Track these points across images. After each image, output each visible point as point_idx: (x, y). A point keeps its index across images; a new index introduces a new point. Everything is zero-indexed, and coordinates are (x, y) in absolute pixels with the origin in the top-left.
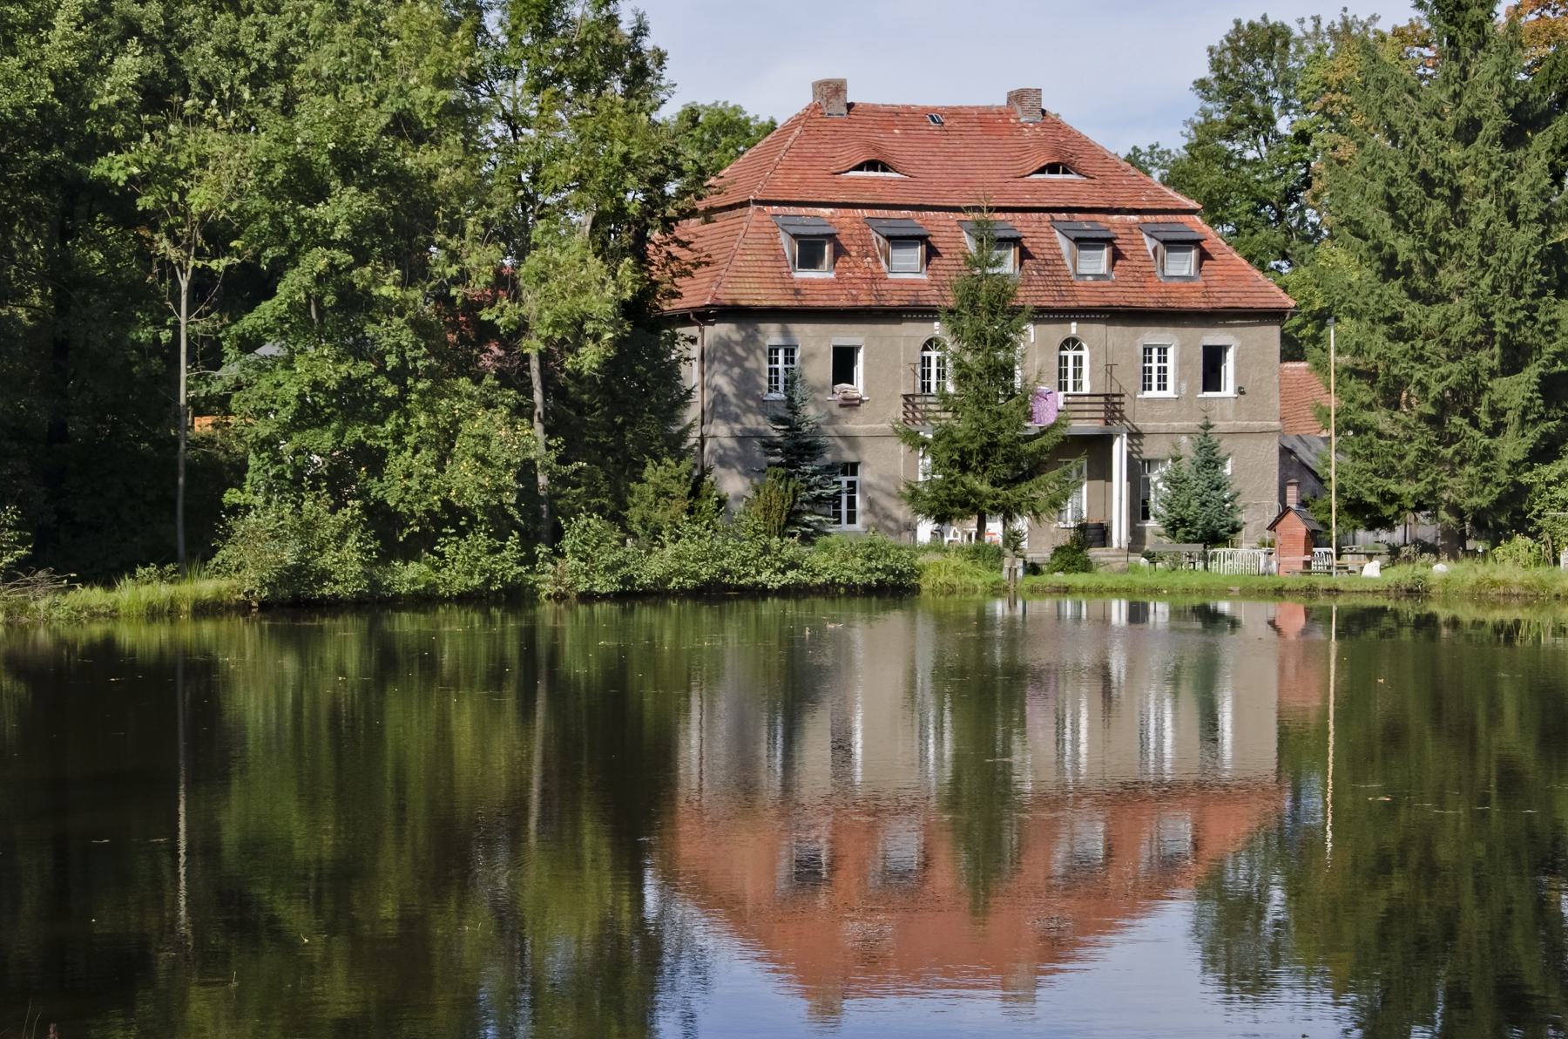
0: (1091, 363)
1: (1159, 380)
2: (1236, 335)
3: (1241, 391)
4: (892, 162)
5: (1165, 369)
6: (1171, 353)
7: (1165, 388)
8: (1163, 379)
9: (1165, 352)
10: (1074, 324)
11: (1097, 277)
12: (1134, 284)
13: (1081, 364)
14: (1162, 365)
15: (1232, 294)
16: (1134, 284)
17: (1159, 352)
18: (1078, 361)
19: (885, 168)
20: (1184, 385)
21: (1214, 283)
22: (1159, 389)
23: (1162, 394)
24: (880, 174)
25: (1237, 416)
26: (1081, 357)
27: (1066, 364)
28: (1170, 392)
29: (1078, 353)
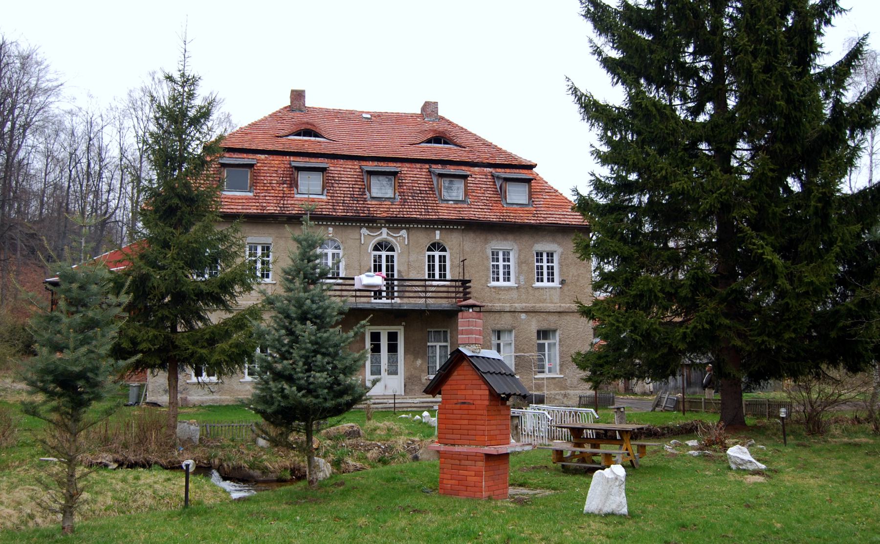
0: (451, 260)
1: (548, 275)
2: (559, 244)
3: (563, 282)
4: (323, 133)
5: (552, 268)
6: (556, 258)
7: (553, 281)
8: (508, 274)
9: (552, 256)
10: (438, 232)
11: (457, 202)
12: (484, 207)
13: (445, 262)
14: (506, 263)
15: (555, 216)
16: (484, 207)
17: (548, 256)
18: (442, 259)
19: (317, 135)
20: (522, 278)
21: (357, 190)
22: (504, 280)
23: (507, 284)
24: (313, 139)
25: (562, 300)
26: (444, 257)
27: (434, 261)
28: (512, 283)
29: (442, 253)
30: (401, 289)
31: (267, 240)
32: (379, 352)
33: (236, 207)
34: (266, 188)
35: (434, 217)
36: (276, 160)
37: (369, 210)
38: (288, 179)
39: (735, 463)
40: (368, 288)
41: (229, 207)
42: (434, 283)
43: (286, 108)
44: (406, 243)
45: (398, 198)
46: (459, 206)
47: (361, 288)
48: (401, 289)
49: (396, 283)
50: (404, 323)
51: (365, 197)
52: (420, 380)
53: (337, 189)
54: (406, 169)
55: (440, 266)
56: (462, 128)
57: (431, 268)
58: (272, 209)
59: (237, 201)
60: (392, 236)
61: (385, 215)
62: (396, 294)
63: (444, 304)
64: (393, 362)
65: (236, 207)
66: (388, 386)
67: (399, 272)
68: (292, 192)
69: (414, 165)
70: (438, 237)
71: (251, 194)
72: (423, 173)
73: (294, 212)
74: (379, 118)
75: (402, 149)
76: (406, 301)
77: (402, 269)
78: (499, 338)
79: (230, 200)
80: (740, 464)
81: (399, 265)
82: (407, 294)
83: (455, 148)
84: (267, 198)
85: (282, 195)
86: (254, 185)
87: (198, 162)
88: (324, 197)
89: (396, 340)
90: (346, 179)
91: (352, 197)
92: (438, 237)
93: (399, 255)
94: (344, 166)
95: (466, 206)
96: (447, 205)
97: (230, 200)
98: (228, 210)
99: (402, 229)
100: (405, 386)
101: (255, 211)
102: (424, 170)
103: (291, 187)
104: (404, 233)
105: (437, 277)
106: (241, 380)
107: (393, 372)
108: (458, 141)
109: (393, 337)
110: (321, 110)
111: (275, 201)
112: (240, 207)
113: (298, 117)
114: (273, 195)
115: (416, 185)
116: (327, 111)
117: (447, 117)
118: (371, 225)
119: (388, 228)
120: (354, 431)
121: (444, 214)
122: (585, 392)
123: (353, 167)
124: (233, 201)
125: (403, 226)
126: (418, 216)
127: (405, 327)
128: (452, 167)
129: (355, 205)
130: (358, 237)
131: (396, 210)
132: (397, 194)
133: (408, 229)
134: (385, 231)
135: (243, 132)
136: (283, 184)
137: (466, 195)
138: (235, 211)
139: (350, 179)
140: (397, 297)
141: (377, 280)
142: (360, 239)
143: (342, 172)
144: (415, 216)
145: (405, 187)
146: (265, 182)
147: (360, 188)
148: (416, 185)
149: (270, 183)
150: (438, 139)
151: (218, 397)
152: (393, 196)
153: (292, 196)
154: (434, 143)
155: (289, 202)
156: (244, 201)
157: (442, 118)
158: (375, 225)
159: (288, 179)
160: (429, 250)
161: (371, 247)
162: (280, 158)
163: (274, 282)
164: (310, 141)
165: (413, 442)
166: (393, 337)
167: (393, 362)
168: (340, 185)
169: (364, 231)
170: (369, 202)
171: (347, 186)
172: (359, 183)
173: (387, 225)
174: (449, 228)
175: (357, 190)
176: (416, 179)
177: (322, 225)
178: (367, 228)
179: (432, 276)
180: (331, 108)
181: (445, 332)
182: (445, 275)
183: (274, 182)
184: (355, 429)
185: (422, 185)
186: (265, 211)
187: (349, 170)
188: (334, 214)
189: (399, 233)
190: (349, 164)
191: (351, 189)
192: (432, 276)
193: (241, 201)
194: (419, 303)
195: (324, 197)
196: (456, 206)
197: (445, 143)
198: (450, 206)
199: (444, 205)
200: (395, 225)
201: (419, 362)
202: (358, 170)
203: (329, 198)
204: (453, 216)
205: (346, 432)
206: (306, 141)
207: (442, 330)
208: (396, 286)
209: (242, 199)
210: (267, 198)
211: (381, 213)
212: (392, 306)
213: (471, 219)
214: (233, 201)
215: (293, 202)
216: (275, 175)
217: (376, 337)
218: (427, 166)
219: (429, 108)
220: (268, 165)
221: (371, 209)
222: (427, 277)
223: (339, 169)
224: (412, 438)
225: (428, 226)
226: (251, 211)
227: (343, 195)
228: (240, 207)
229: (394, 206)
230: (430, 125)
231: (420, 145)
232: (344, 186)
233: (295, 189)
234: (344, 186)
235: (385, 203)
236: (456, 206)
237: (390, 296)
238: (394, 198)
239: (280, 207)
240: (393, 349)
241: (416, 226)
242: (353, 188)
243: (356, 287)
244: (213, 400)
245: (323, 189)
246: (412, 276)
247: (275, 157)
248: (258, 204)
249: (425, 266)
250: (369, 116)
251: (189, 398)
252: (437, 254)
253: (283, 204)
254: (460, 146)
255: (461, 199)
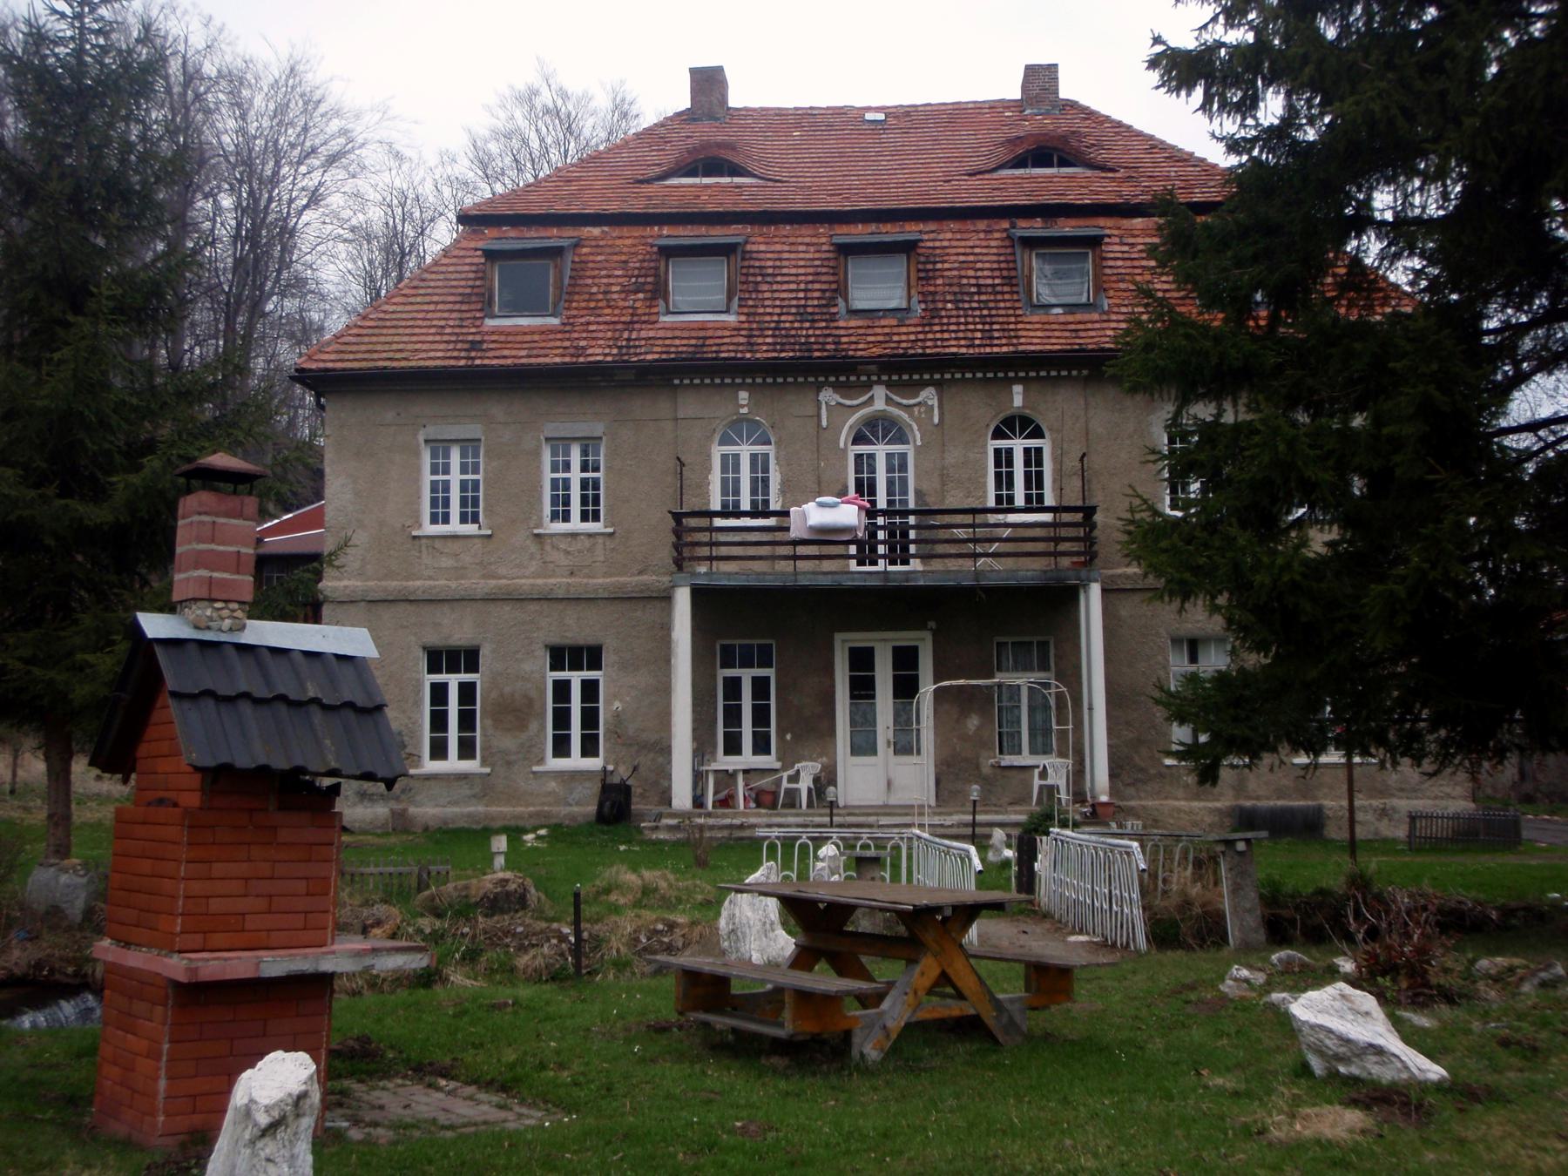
4: (751, 166)
10: (1018, 389)
13: (1039, 463)
19: (736, 171)
26: (1039, 451)
29: (1033, 443)
30: (926, 534)
31: (598, 429)
32: (873, 697)
33: (514, 353)
34: (592, 305)
35: (1005, 349)
36: (627, 239)
37: (839, 343)
38: (649, 280)
39: (1320, 1052)
40: (826, 537)
41: (497, 353)
42: (1013, 518)
43: (678, 114)
44: (936, 420)
45: (919, 309)
46: (1079, 317)
47: (806, 536)
48: (926, 534)
49: (880, 521)
50: (932, 624)
51: (834, 310)
52: (978, 767)
53: (767, 295)
54: (949, 236)
55: (1027, 475)
56: (1119, 124)
57: (1004, 480)
58: (598, 353)
59: (519, 338)
60: (899, 405)
61: (877, 351)
62: (912, 549)
63: (1030, 570)
64: (904, 721)
65: (514, 353)
66: (896, 783)
67: (918, 493)
68: (654, 310)
69: (969, 226)
70: (1018, 401)
71: (555, 321)
72: (993, 243)
73: (649, 357)
74: (906, 119)
75: (947, 187)
76: (937, 565)
77: (925, 487)
78: (1193, 659)
79: (502, 338)
80: (1339, 1058)
81: (917, 476)
82: (940, 549)
83: (1089, 173)
84: (592, 328)
85: (627, 319)
86: (568, 294)
87: (86, 207)
88: (731, 318)
89: (915, 666)
90: (794, 271)
91: (802, 315)
92: (1018, 401)
93: (918, 450)
94: (792, 240)
95: (1096, 316)
96: (1044, 318)
97: (502, 338)
98: (495, 362)
99: (923, 384)
100: (938, 782)
101: (558, 360)
102: (997, 235)
103: (654, 298)
104: (929, 395)
105: (1020, 501)
106: (535, 768)
107: (905, 746)
108: (1101, 156)
109: (905, 660)
110: (764, 112)
111: (609, 334)
112: (524, 353)
113: (705, 132)
114: (608, 318)
115: (971, 273)
116: (780, 113)
117: (1084, 101)
118: (842, 379)
119: (889, 385)
120: (508, 894)
121: (1033, 341)
122: (1444, 803)
123: (814, 240)
124: (510, 338)
125: (927, 377)
126: (964, 350)
127: (935, 634)
128: (1073, 222)
129: (806, 332)
130: (811, 411)
131: (906, 339)
132: (915, 300)
133: (939, 385)
134: (879, 392)
135: (562, 177)
136: (636, 292)
137: (1100, 288)
138: (509, 362)
139: (802, 271)
140: (914, 556)
141: (847, 514)
142: (819, 416)
143: (786, 255)
144: (954, 350)
145: (940, 281)
146: (594, 290)
147: (823, 291)
148: (971, 273)
149: (605, 293)
150: (1043, 152)
151: (481, 809)
152: (904, 305)
153: (653, 318)
154: (1034, 166)
155: (643, 334)
156: (536, 337)
157: (1072, 105)
158: (853, 378)
159: (649, 280)
160: (998, 434)
161: (844, 437)
162: (637, 232)
163: (610, 530)
164: (717, 185)
165: (672, 926)
166: (905, 660)
167: (904, 721)
168: (775, 287)
169: (828, 396)
170: (841, 324)
171: (793, 286)
172: (824, 278)
173: (885, 378)
174: (1048, 377)
175: (817, 294)
176: (971, 258)
177: (722, 385)
178: (837, 387)
179: (1005, 504)
180: (791, 106)
181: (1043, 646)
182: (1040, 498)
183: (615, 289)
184: (512, 887)
185: (986, 273)
186: (581, 360)
187: (801, 248)
188: (748, 355)
189: (916, 396)
190: (805, 234)
191: (801, 295)
192: (1005, 504)
193: (528, 338)
194: (953, 570)
195: (731, 318)
196: (1070, 318)
197: (1064, 163)
198: (1052, 319)
199: (1035, 319)
200: (905, 377)
201: (973, 722)
202: (825, 248)
203: (743, 318)
204: (1057, 343)
205: (485, 896)
206: (707, 186)
207: (1035, 639)
208: (913, 527)
209: (533, 333)
210: (592, 328)
211: (866, 348)
212: (887, 580)
213: (1103, 350)
214: (510, 338)
215: (651, 334)
216: (620, 273)
217: (862, 660)
218: (1005, 225)
219: (1041, 79)
220: (608, 250)
221: (844, 340)
222: (991, 503)
223: (778, 247)
224: (671, 917)
225: (990, 375)
226: (547, 360)
227: (778, 310)
228: (524, 353)
229: (904, 330)
230: (1037, 123)
231: (995, 175)
232: (785, 287)
233: (661, 302)
234: (785, 287)
235: (883, 322)
236: (1070, 318)
237: (898, 554)
238: (908, 310)
239: (620, 348)
240: (906, 688)
241: (958, 376)
242: (805, 291)
243: (794, 533)
244: (469, 815)
245: (730, 299)
246: (952, 502)
247: (625, 231)
248: (567, 344)
249: (985, 475)
250: (881, 117)
251: (412, 810)
252: (1018, 445)
253: (628, 340)
254: (1103, 168)
255: (1084, 300)
